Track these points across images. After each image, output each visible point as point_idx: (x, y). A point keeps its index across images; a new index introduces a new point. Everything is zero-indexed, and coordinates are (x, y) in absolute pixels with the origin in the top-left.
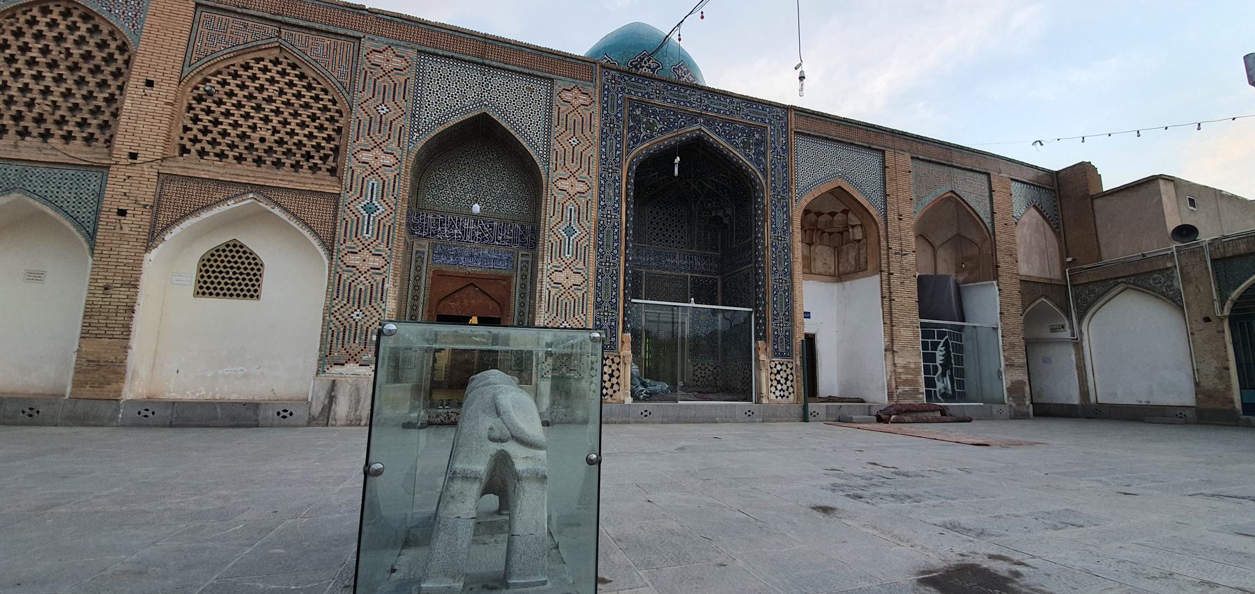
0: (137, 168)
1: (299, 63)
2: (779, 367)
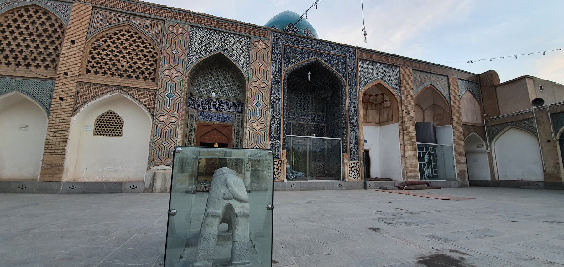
0: (68, 79)
1: (138, 32)
2: (353, 165)
